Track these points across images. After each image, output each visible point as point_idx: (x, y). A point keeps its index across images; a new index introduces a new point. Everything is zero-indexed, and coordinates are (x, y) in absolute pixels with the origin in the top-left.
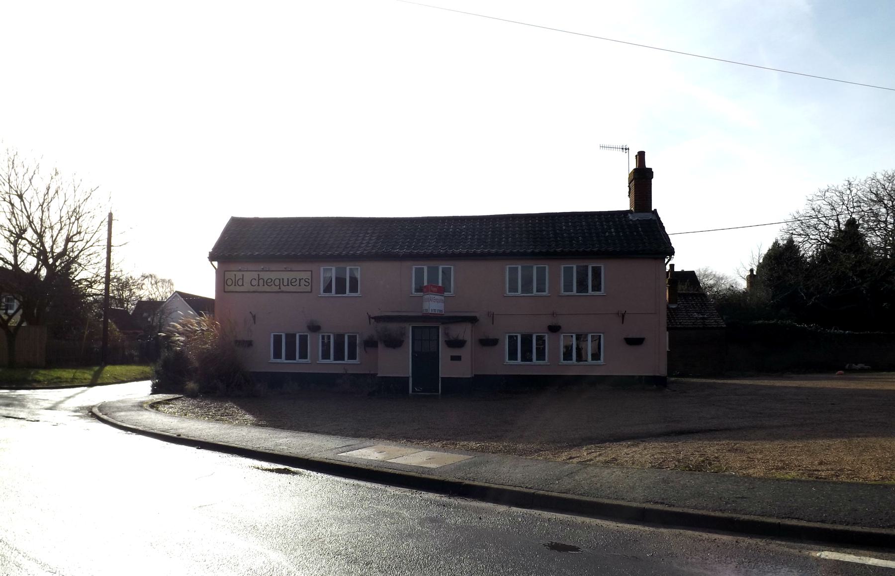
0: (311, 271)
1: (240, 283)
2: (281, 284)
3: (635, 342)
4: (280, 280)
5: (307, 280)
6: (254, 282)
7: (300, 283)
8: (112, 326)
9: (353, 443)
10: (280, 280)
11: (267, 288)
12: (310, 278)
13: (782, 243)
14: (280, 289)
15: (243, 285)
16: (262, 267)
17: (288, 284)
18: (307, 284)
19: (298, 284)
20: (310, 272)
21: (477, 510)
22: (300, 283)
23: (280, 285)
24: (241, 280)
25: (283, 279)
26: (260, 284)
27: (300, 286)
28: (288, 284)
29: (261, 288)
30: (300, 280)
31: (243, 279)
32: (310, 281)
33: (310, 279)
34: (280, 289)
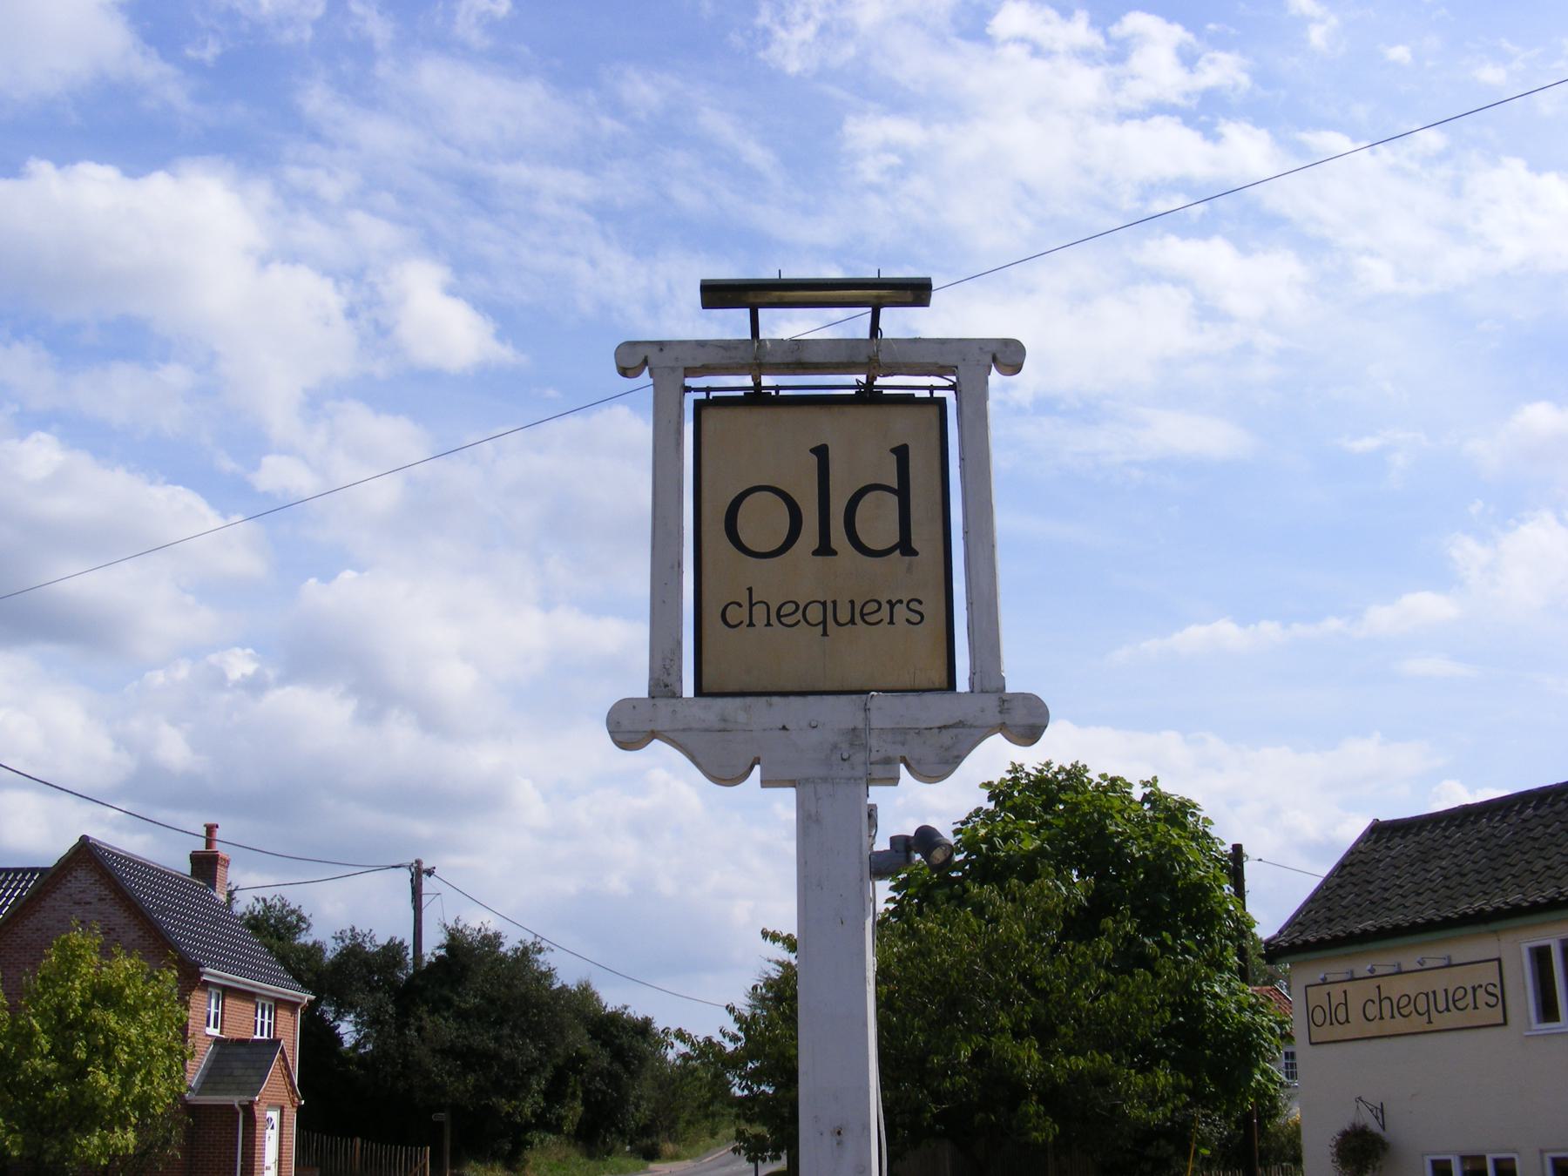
0: (1499, 960)
1: (1342, 1018)
2: (1432, 1004)
3: (880, 709)
4: (1427, 995)
5: (1491, 989)
6: (1372, 1011)
7: (1381, 1013)
8: (686, 1154)
9: (1133, 132)
10: (1427, 995)
11: (1400, 1024)
12: (1497, 982)
13: (508, 946)
14: (1430, 1022)
15: (1347, 1021)
16: (1369, 967)
17: (1447, 1005)
18: (1492, 1000)
19: (1472, 1005)
20: (1496, 963)
21: (292, 1134)
22: (1381, 1013)
23: (1428, 1010)
24: (1342, 1009)
25: (1434, 992)
26: (1384, 1016)
27: (1476, 1007)
28: (1447, 1005)
29: (1389, 1026)
30: (1474, 989)
31: (1346, 1004)
32: (1497, 991)
33: (1499, 986)
34: (1430, 1022)
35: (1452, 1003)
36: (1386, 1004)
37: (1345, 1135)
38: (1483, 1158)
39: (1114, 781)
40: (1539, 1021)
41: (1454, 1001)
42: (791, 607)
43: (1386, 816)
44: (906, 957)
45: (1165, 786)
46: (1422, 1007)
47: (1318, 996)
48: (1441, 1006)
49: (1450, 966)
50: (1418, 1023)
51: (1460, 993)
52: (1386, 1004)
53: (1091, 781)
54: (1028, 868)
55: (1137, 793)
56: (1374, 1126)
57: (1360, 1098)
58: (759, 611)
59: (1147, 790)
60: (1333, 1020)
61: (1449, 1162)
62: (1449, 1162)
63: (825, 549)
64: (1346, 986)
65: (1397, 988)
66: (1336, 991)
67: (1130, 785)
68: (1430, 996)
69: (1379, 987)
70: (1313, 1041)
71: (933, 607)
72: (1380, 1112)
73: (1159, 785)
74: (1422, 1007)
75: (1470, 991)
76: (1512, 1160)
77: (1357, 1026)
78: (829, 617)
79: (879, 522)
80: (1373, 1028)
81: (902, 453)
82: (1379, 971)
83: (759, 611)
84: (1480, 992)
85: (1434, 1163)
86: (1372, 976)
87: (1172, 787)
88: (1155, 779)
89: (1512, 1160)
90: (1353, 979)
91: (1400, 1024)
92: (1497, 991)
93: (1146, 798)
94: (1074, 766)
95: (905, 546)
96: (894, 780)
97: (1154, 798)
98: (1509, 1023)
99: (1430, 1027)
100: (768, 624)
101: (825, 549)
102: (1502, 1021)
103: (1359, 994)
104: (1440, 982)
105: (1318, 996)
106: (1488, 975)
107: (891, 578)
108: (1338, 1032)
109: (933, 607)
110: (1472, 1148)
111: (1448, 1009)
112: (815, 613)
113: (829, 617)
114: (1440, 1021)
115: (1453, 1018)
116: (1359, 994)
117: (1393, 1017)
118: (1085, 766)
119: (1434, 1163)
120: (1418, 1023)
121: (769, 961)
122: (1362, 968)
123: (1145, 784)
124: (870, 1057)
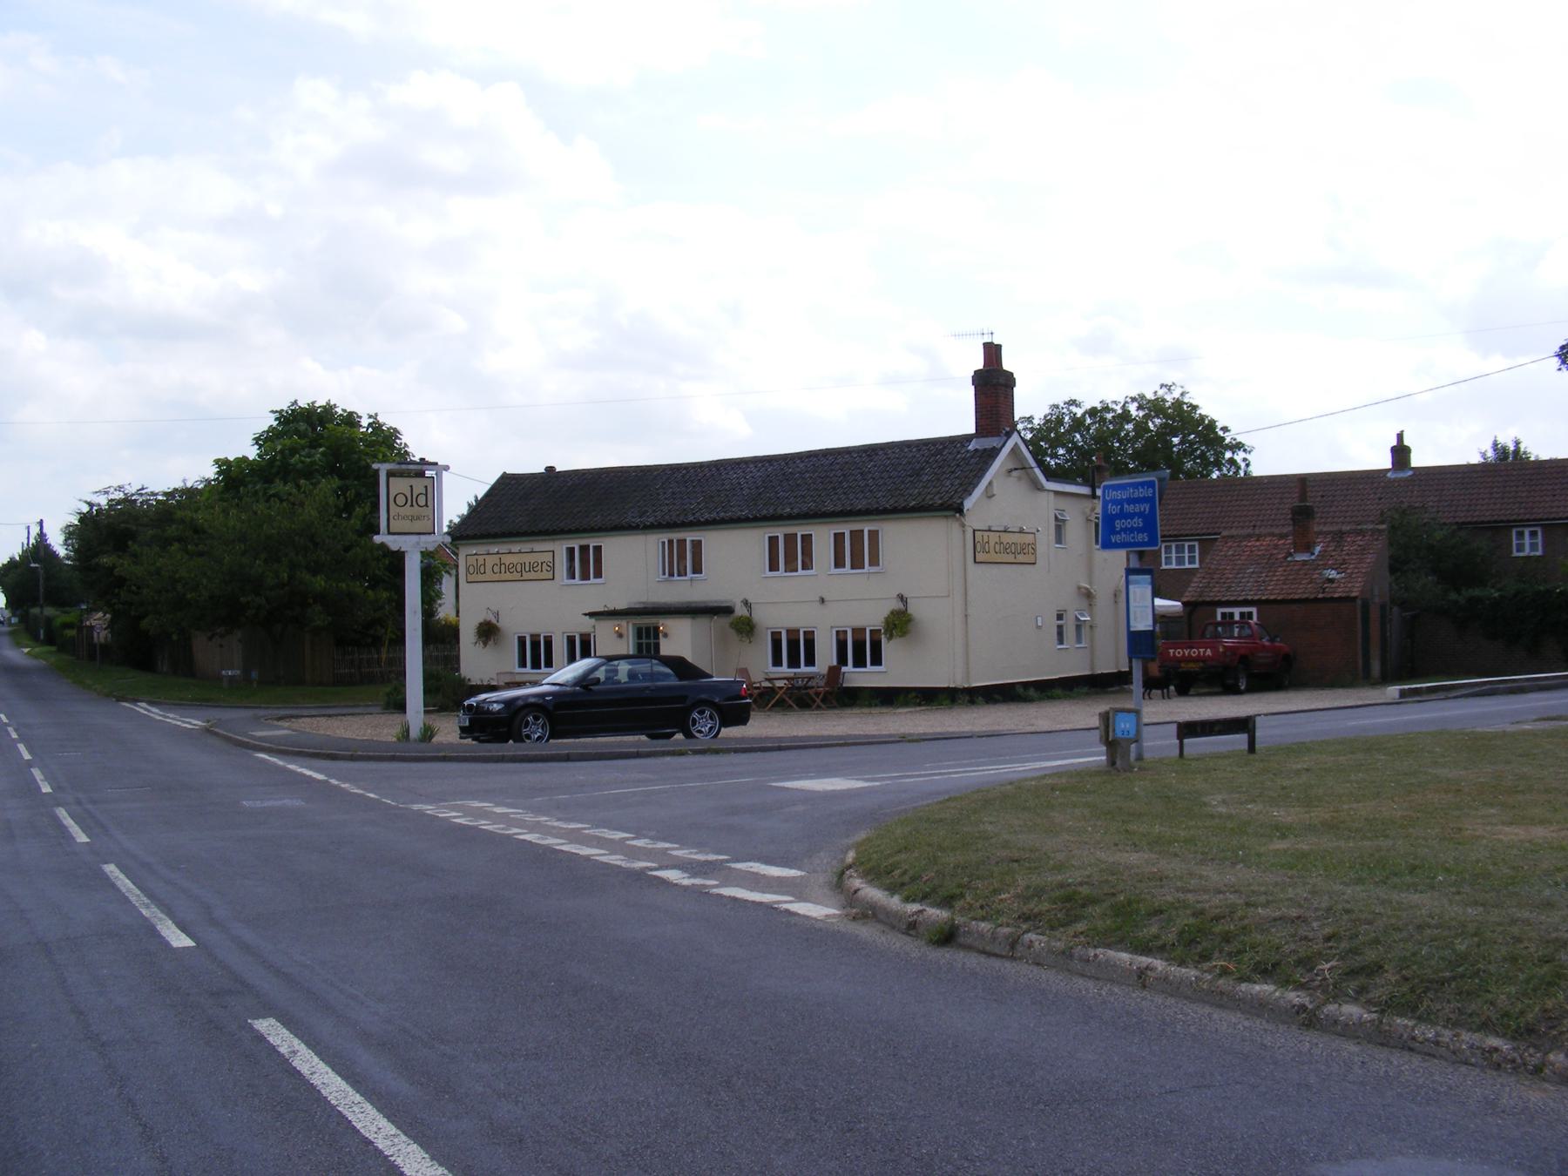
6: (496, 569)
12: (551, 561)
15: (485, 573)
18: (549, 569)
20: (551, 553)
24: (482, 567)
32: (551, 565)
35: (532, 568)
36: (503, 566)
37: (481, 624)
38: (539, 636)
39: (351, 414)
40: (567, 579)
43: (510, 471)
45: (381, 419)
46: (519, 570)
47: (472, 560)
48: (527, 569)
49: (532, 552)
51: (536, 564)
52: (503, 566)
53: (336, 412)
54: (309, 473)
55: (365, 422)
56: (494, 621)
59: (371, 420)
61: (525, 637)
62: (525, 637)
63: (412, 505)
65: (508, 559)
66: (481, 559)
67: (361, 417)
71: (431, 517)
72: (497, 615)
73: (378, 418)
74: (519, 570)
76: (551, 636)
77: (489, 575)
78: (412, 519)
79: (422, 501)
80: (496, 577)
81: (426, 487)
82: (501, 552)
84: (544, 565)
85: (519, 637)
86: (498, 553)
87: (388, 421)
88: (376, 414)
89: (551, 636)
90: (488, 554)
91: (508, 576)
92: (551, 565)
93: (370, 425)
94: (328, 404)
95: (426, 505)
97: (376, 426)
101: (412, 505)
103: (491, 560)
104: (527, 559)
105: (472, 560)
106: (548, 557)
107: (424, 511)
108: (481, 577)
109: (431, 517)
110: (535, 631)
113: (412, 519)
114: (526, 576)
115: (532, 575)
116: (491, 560)
118: (335, 405)
119: (519, 637)
120: (516, 576)
121: (80, 500)
123: (370, 417)
124: (1351, 691)
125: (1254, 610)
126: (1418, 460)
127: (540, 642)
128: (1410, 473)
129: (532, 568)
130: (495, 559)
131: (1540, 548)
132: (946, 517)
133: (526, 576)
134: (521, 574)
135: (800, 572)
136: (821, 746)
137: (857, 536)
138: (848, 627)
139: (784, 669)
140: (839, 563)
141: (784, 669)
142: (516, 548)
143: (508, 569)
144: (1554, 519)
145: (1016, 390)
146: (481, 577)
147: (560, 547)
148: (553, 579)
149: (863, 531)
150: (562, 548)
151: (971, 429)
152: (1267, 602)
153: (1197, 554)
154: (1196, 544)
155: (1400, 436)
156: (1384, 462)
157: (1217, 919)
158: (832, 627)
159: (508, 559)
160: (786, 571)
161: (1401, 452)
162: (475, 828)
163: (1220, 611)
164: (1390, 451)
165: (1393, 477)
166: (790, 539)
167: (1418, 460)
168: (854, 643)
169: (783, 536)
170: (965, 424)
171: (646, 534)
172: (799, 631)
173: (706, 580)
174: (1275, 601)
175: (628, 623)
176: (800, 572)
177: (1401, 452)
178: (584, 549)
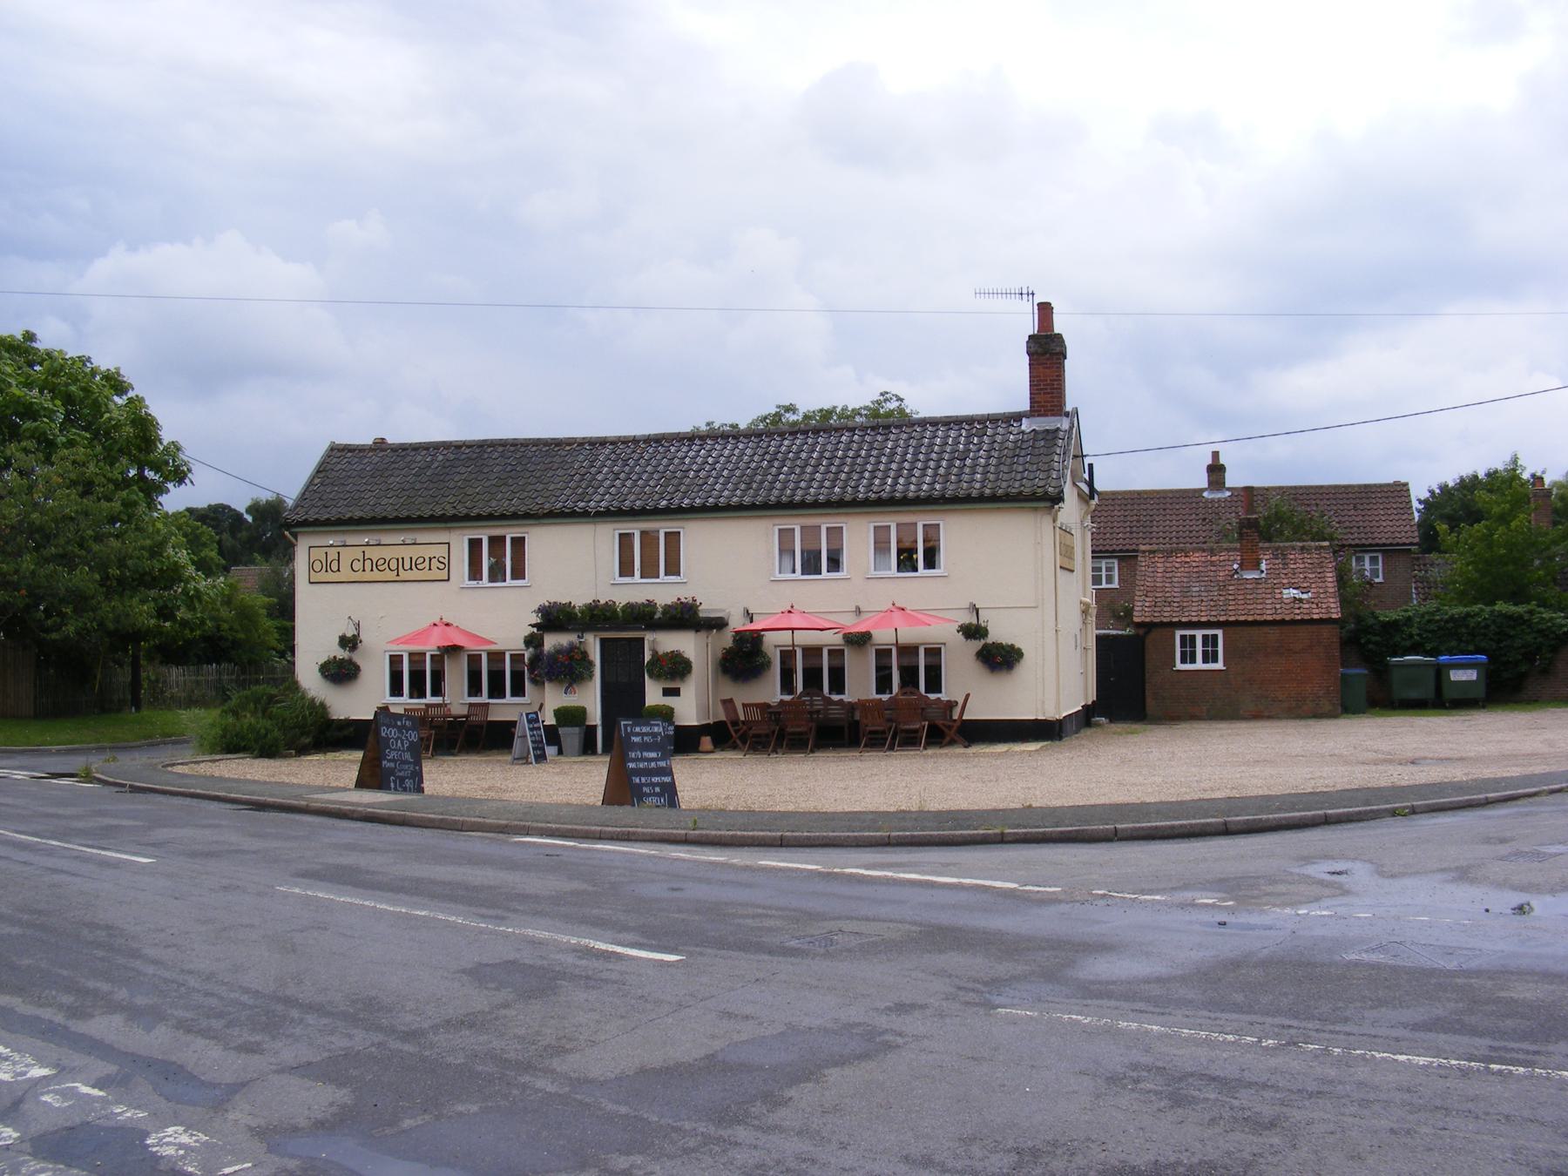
0: (449, 544)
4: (398, 560)
5: (441, 559)
6: (357, 566)
10: (398, 560)
11: (376, 575)
14: (398, 575)
15: (339, 570)
18: (442, 566)
23: (398, 568)
29: (368, 576)
33: (447, 558)
34: (398, 575)
35: (414, 565)
41: (416, 565)
42: (382, 561)
44: (108, 574)
50: (392, 576)
57: (350, 617)
58: (368, 563)
60: (327, 567)
64: (339, 549)
66: (333, 553)
68: (400, 561)
69: (364, 552)
70: (311, 581)
74: (394, 566)
75: (427, 560)
77: (346, 573)
83: (368, 563)
91: (376, 575)
96: (168, 491)
98: (451, 580)
99: (398, 579)
100: (372, 570)
102: (447, 578)
105: (318, 554)
106: (441, 551)
108: (331, 576)
111: (411, 569)
112: (393, 565)
114: (404, 575)
117: (372, 570)
120: (392, 576)
122: (351, 540)
125: (1219, 633)
126: (1235, 478)
127: (821, 669)
128: (1228, 494)
129: (414, 565)
130: (358, 553)
131: (1381, 575)
132: (1036, 509)
133: (404, 575)
134: (398, 574)
135: (509, 581)
136: (1487, 803)
137: (811, 533)
138: (405, 651)
139: (405, 699)
140: (475, 573)
141: (405, 699)
142: (386, 539)
143: (376, 566)
144: (1398, 544)
145: (1067, 362)
146: (331, 576)
147: (459, 542)
148: (448, 580)
149: (504, 538)
150: (774, 532)
151: (1025, 406)
152: (1237, 623)
153: (1380, 566)
154: (1116, 561)
155: (1216, 455)
156: (1200, 481)
157: (1495, 973)
158: (385, 651)
159: (374, 552)
160: (802, 574)
161: (1216, 470)
162: (434, 918)
163: (1179, 633)
164: (1205, 470)
165: (1210, 497)
166: (648, 539)
167: (1235, 478)
168: (412, 673)
169: (639, 533)
170: (1020, 400)
171: (595, 523)
172: (425, 654)
173: (685, 583)
174: (1245, 623)
175: (595, 636)
176: (509, 581)
177: (1216, 470)
178: (496, 542)
